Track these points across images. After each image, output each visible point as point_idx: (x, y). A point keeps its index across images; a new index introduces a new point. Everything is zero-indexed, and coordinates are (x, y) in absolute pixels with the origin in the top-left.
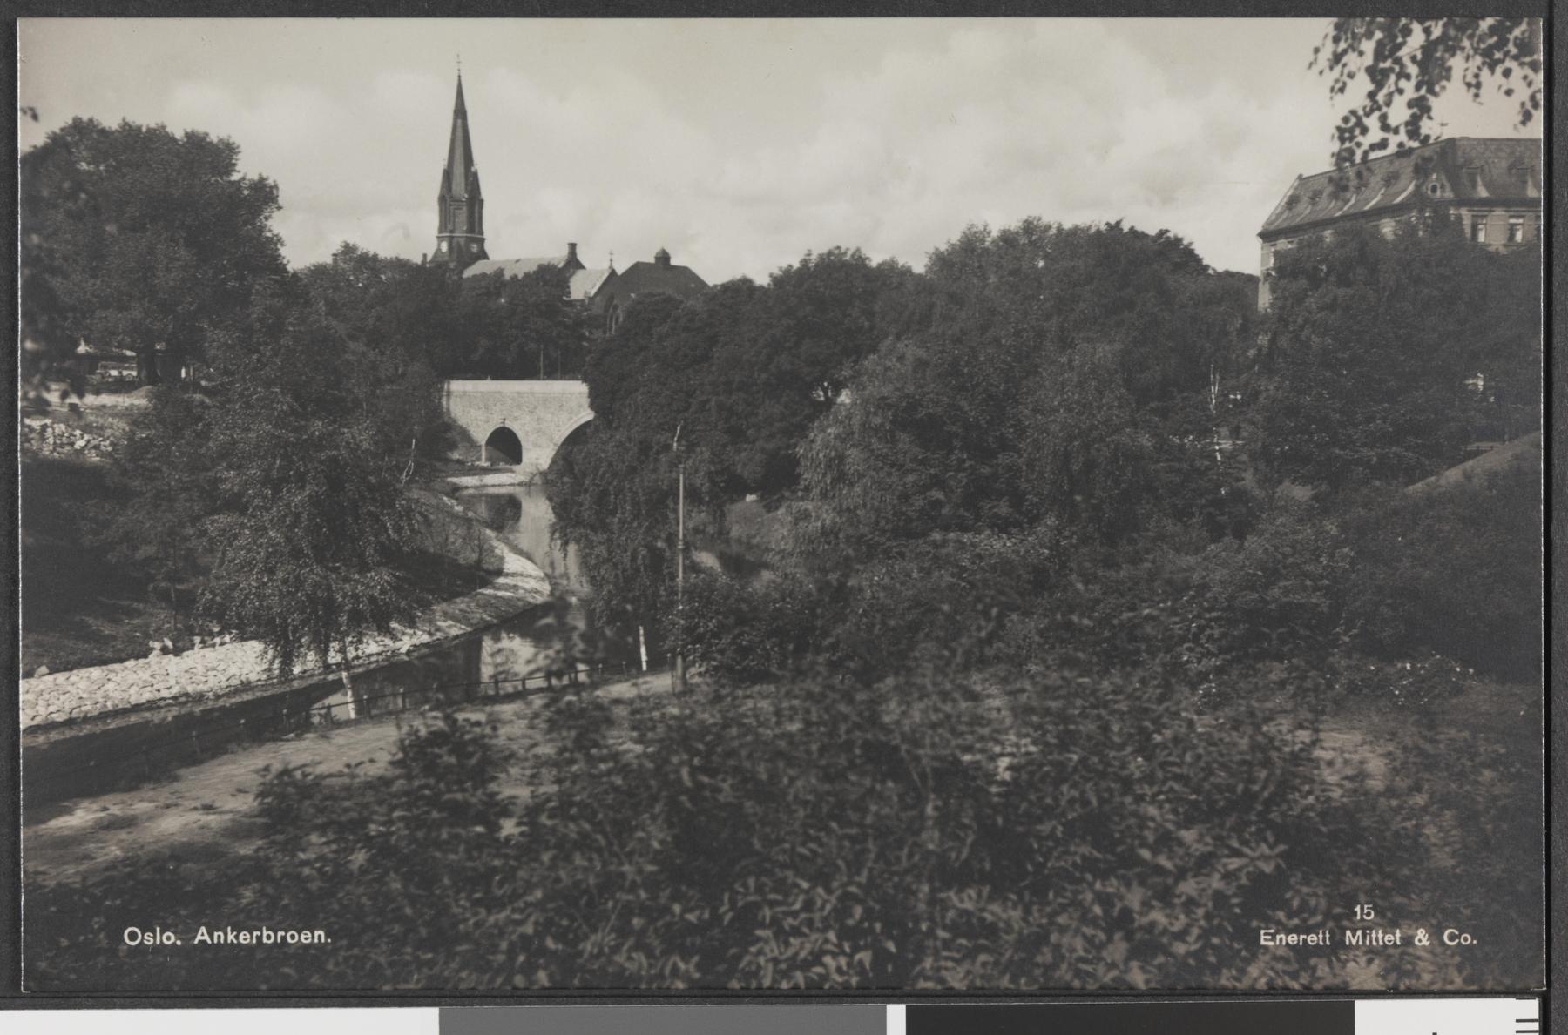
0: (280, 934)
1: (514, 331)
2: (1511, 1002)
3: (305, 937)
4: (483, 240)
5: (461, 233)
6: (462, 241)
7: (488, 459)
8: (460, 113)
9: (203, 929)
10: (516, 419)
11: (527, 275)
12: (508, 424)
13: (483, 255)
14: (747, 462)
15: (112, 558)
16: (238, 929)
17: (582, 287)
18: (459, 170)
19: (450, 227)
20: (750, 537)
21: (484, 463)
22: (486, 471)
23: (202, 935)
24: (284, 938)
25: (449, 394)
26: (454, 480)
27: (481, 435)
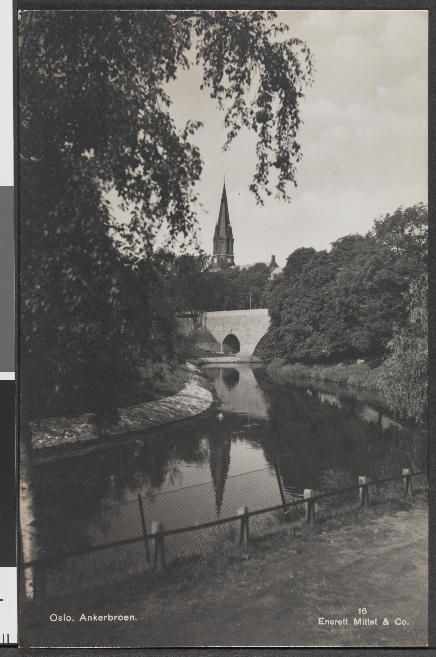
0: (116, 617)
1: (243, 293)
2: (16, 632)
3: (126, 618)
4: (233, 257)
5: (223, 254)
6: (223, 258)
7: (223, 351)
8: (224, 200)
9: (83, 615)
10: (237, 330)
11: (250, 268)
12: (234, 333)
14: (358, 338)
16: (98, 615)
18: (223, 225)
19: (218, 251)
20: (360, 382)
21: (222, 353)
22: (220, 355)
23: (83, 617)
24: (117, 618)
25: (206, 318)
26: (203, 359)
27: (220, 338)
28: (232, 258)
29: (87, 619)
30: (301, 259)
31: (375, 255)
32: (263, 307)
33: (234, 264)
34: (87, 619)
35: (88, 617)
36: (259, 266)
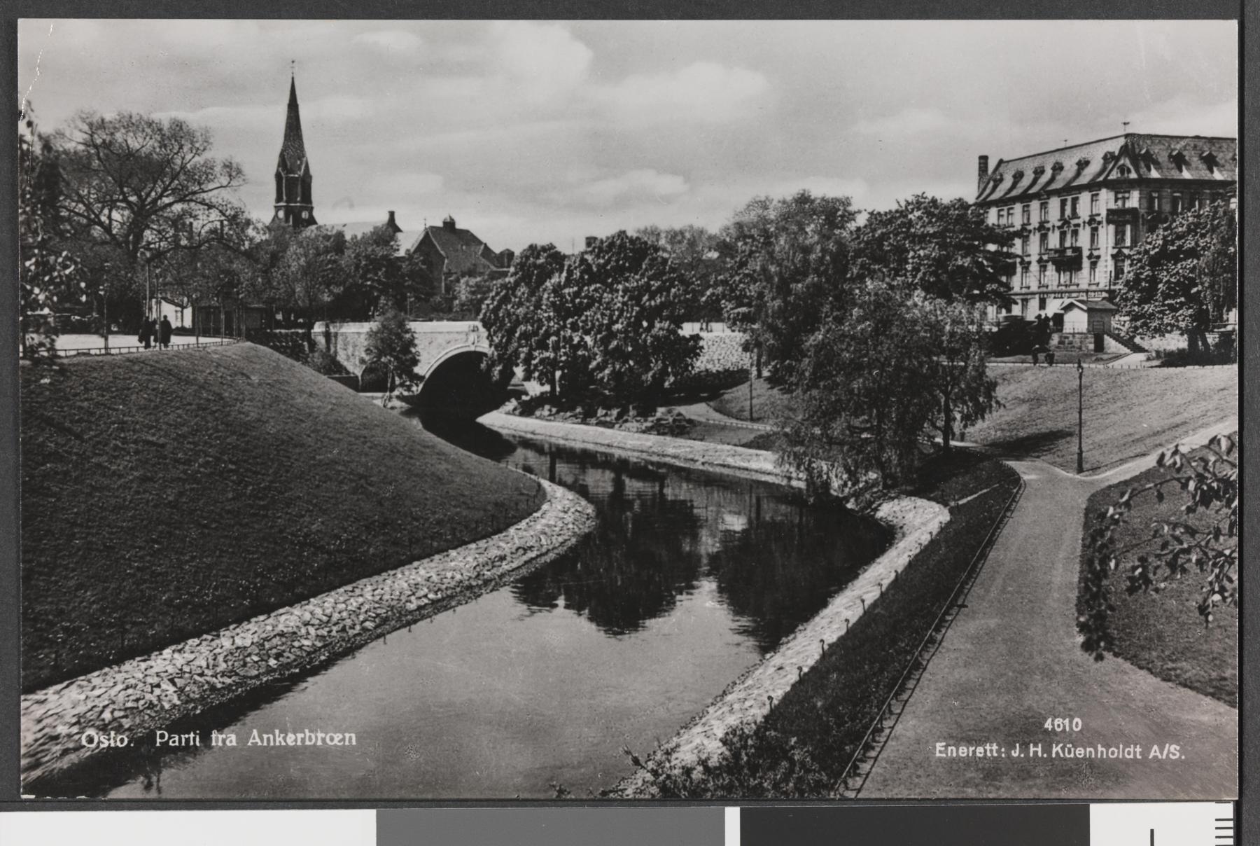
8: (293, 106)
9: (1155, 747)
13: (311, 221)
15: (615, 412)
17: (406, 243)
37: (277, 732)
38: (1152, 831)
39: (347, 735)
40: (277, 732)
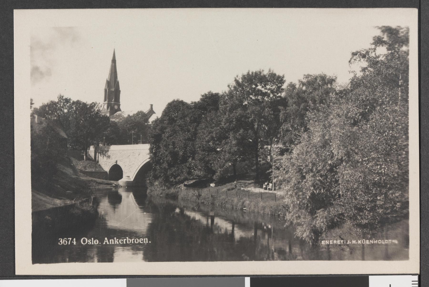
4: (120, 105)
8: (114, 61)
28: (119, 105)
29: (109, 242)
30: (176, 108)
31: (211, 134)
32: (143, 143)
33: (120, 110)
34: (109, 242)
35: (110, 240)
36: (140, 113)
37: (115, 238)
38: (390, 285)
39: (145, 239)
40: (115, 238)
